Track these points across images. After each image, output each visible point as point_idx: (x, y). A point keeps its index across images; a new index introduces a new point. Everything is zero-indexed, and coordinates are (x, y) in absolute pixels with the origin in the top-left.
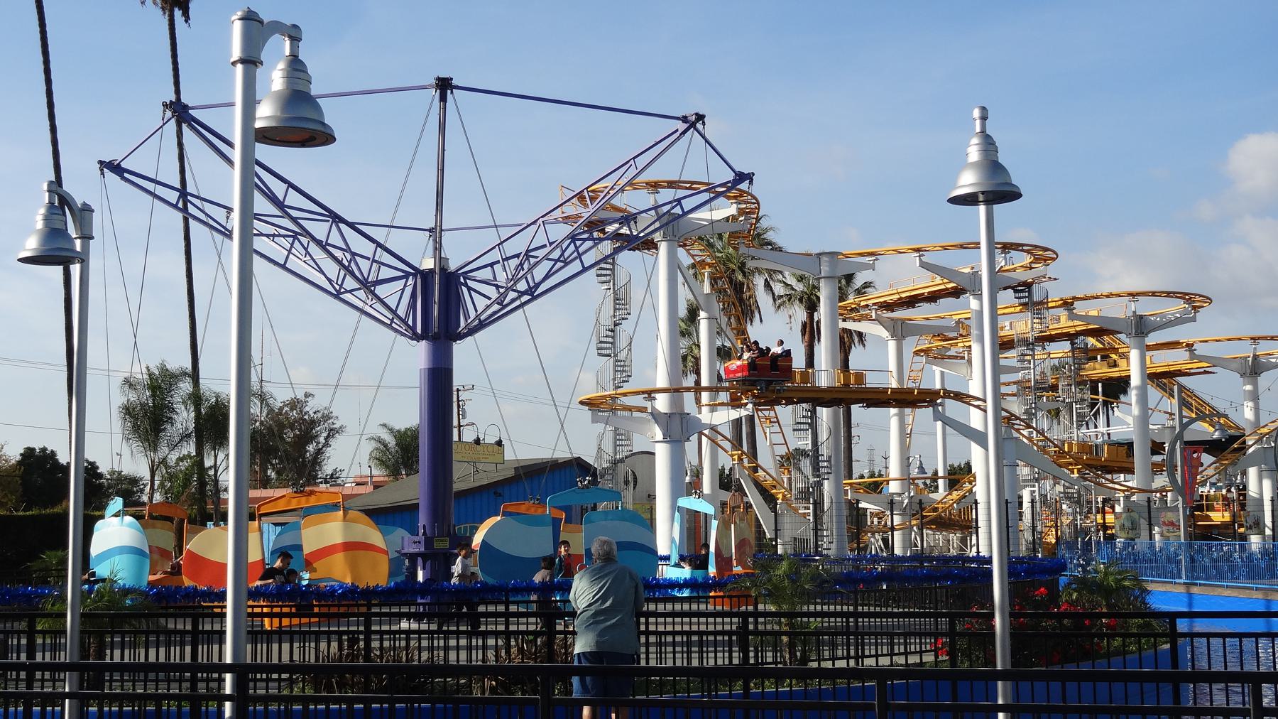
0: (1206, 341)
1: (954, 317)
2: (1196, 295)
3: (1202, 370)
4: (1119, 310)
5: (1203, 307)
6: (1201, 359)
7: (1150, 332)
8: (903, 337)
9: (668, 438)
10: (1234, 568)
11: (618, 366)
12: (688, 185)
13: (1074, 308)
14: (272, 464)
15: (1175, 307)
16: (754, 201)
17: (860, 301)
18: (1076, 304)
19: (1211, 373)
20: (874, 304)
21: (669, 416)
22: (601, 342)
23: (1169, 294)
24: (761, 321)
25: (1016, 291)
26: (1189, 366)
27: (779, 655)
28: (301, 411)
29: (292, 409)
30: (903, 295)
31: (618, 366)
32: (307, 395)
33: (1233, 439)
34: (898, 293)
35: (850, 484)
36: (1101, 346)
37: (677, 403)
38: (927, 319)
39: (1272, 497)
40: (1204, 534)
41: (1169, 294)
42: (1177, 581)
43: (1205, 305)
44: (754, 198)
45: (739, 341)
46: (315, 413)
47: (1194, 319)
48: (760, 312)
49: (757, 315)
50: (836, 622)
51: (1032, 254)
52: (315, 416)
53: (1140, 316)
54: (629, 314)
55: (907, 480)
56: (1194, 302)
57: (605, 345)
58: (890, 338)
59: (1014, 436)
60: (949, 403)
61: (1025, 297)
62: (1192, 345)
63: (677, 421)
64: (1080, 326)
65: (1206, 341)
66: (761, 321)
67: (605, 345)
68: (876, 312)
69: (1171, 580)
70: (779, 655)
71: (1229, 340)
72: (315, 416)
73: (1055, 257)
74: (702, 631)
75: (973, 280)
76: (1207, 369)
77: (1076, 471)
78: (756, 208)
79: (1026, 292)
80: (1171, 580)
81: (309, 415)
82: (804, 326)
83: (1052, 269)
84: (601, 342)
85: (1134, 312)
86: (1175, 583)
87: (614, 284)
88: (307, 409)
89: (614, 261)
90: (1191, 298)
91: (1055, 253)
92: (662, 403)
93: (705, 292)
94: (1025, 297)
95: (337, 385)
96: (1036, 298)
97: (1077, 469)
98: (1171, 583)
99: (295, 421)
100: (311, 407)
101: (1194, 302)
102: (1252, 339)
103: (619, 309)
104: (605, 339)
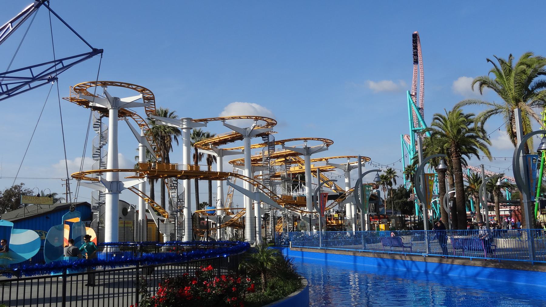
0: (332, 158)
1: (242, 148)
2: (328, 140)
3: (331, 169)
4: (301, 145)
5: (331, 145)
6: (332, 165)
7: (312, 154)
8: (223, 156)
9: (111, 191)
10: (339, 243)
11: (102, 164)
12: (123, 84)
13: (285, 145)
14: (7, 210)
15: (322, 144)
16: (151, 93)
17: (205, 141)
18: (285, 143)
19: (333, 170)
20: (210, 142)
21: (112, 182)
22: (94, 154)
23: (318, 139)
24: (172, 151)
25: (263, 138)
26: (326, 168)
27: (222, 272)
28: (19, 190)
29: (15, 189)
30: (221, 139)
31: (102, 164)
32: (22, 184)
33: (341, 194)
34: (219, 138)
35: (201, 212)
36: (295, 160)
37: (115, 177)
38: (232, 149)
39: (355, 214)
40: (331, 228)
41: (318, 139)
42: (318, 248)
43: (331, 144)
44: (151, 92)
45: (158, 156)
46: (25, 190)
47: (327, 149)
48: (172, 148)
49: (171, 149)
50: (119, 278)
51: (267, 121)
52: (25, 192)
53: (308, 147)
54: (107, 143)
55: (224, 210)
56: (328, 143)
57: (96, 156)
58: (217, 156)
59: (259, 191)
60: (234, 179)
61: (267, 140)
62: (327, 160)
63: (115, 185)
64: (288, 151)
65: (332, 158)
66: (172, 151)
67: (96, 156)
68: (211, 146)
69: (325, 248)
70: (222, 272)
71: (340, 158)
72: (25, 192)
73: (276, 123)
74: (88, 278)
75: (245, 132)
76: (333, 169)
77: (283, 205)
78: (153, 97)
79: (267, 138)
80: (325, 248)
81: (22, 191)
82: (194, 156)
83: (275, 128)
84: (94, 154)
85: (306, 146)
86: (317, 249)
87: (101, 131)
88: (22, 189)
89: (101, 121)
90: (326, 141)
91: (276, 121)
92: (108, 177)
93: (141, 136)
94: (267, 140)
95: (16, 178)
96: (271, 140)
97: (284, 204)
98: (315, 248)
99: (16, 194)
100: (23, 189)
101: (328, 143)
102: (348, 157)
103: (102, 141)
104: (96, 153)
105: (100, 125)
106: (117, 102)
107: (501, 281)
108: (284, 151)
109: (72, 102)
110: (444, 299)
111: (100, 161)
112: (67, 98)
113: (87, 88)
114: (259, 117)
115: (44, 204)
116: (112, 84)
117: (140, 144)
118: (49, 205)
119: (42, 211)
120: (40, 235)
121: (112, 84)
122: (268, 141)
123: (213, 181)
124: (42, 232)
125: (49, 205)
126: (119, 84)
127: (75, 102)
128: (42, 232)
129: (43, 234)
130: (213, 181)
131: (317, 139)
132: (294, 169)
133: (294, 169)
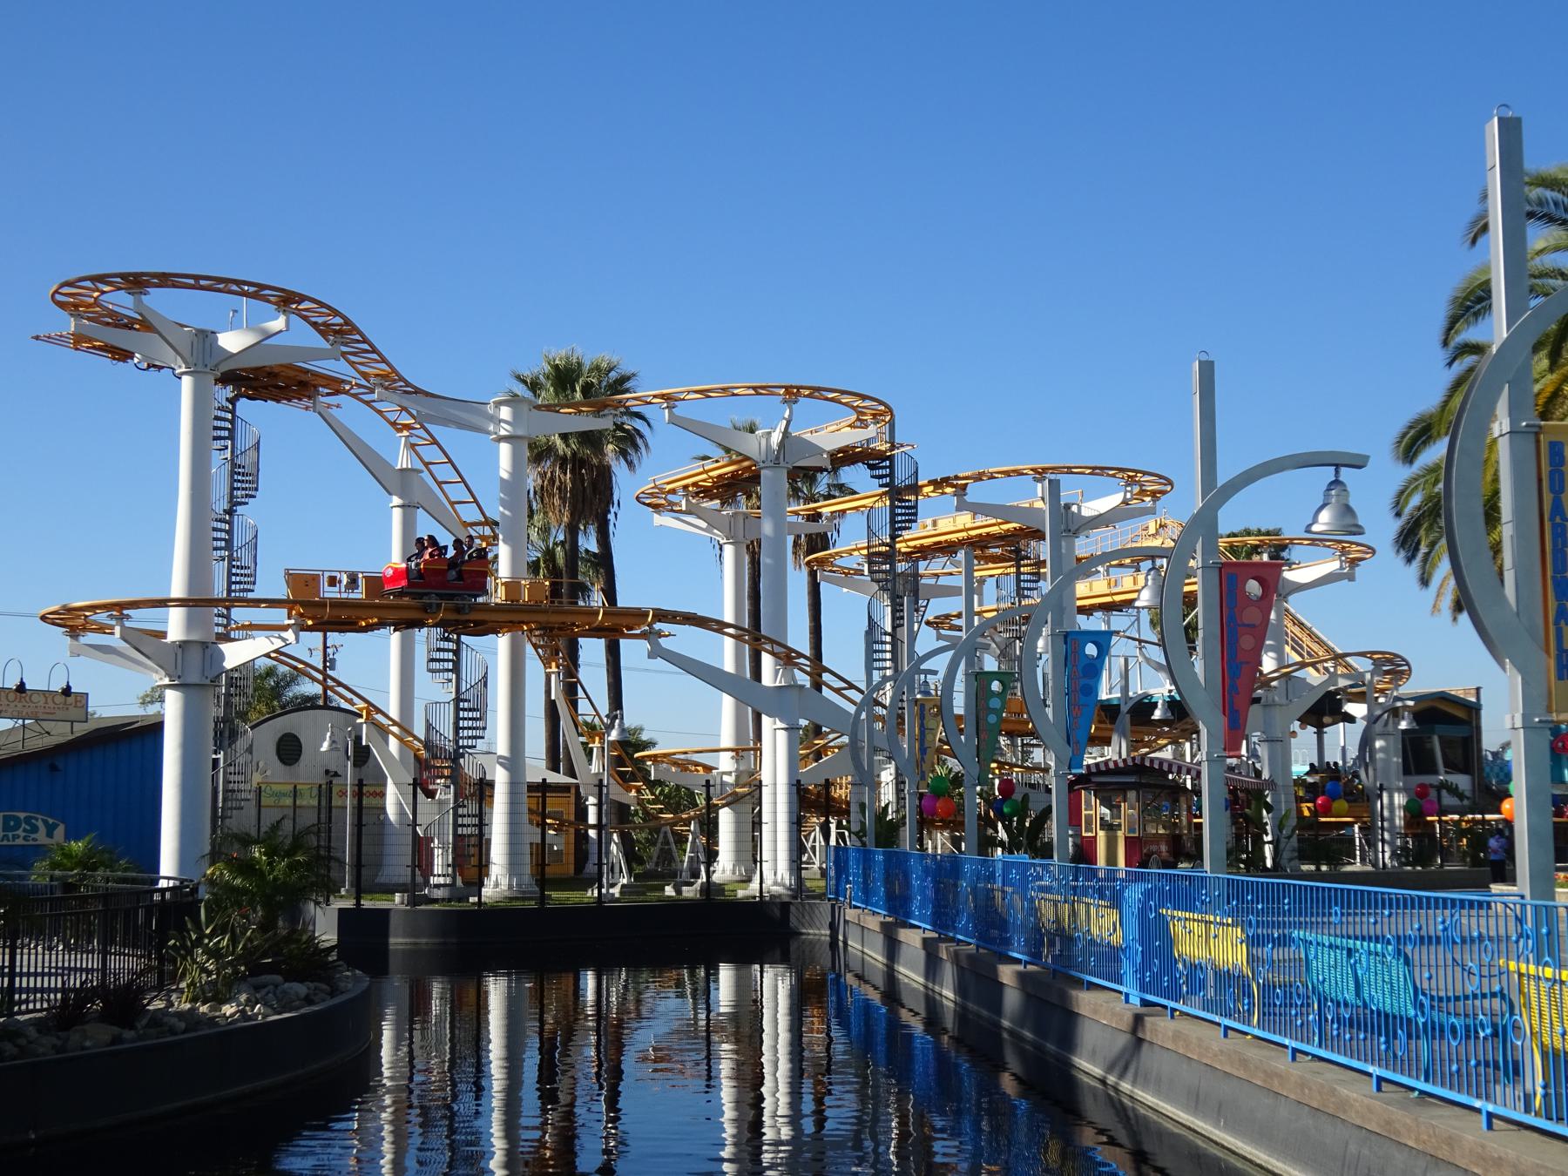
2: (1137, 472)
25: (871, 467)
87: (232, 452)
92: (175, 625)
93: (399, 467)
105: (232, 431)
106: (207, 345)
107: (1053, 1048)
108: (965, 519)
109: (77, 349)
110: (855, 1114)
111: (229, 563)
112: (49, 337)
113: (103, 292)
114: (799, 388)
115: (51, 717)
116: (166, 280)
117: (396, 500)
118: (72, 722)
119: (37, 743)
120: (28, 828)
121: (166, 280)
122: (892, 480)
123: (328, 634)
124: (37, 819)
125: (72, 722)
126: (203, 282)
127: (88, 348)
128: (31, 818)
129: (40, 824)
130: (328, 634)
131: (1088, 471)
132: (1091, 590)
133: (1091, 590)
